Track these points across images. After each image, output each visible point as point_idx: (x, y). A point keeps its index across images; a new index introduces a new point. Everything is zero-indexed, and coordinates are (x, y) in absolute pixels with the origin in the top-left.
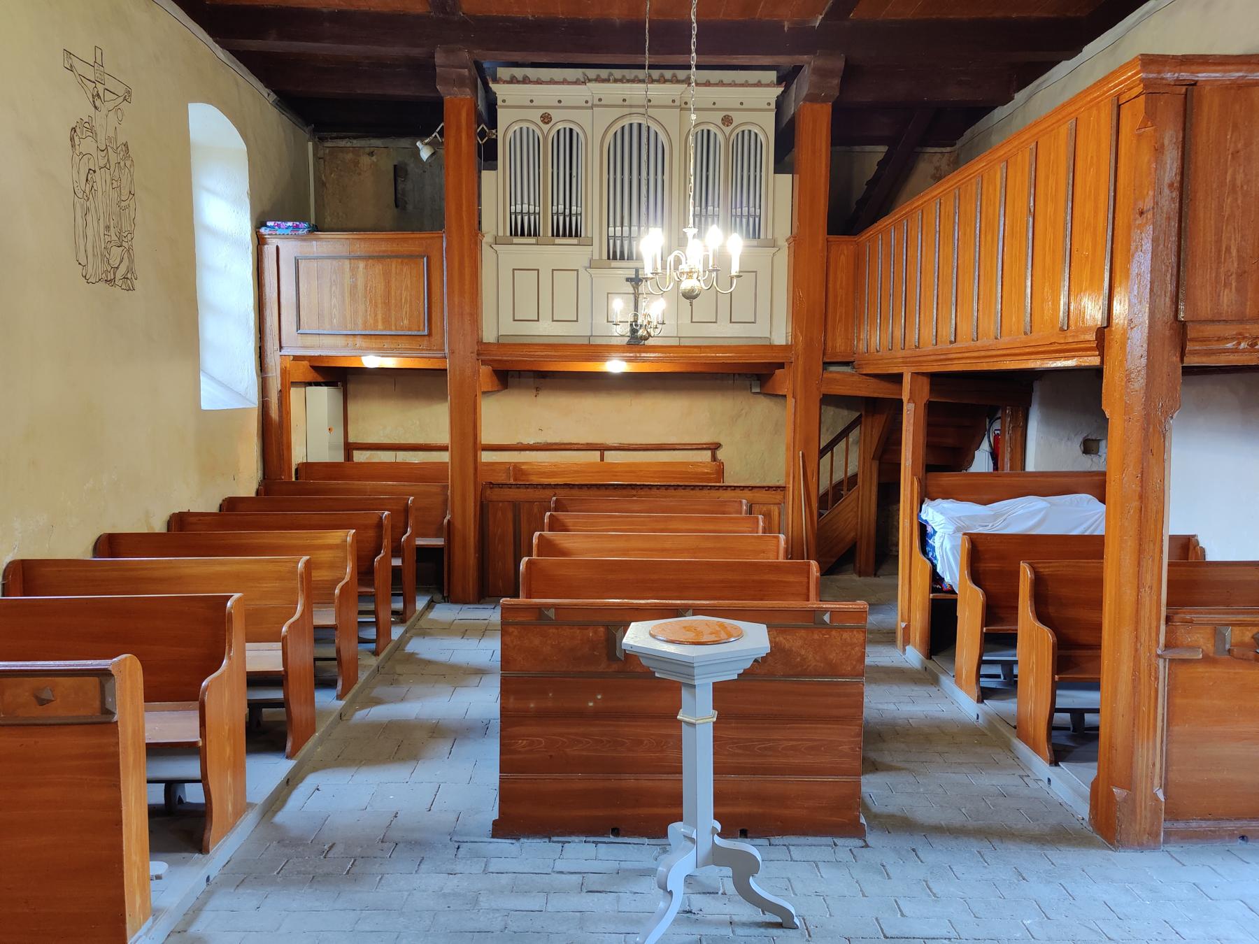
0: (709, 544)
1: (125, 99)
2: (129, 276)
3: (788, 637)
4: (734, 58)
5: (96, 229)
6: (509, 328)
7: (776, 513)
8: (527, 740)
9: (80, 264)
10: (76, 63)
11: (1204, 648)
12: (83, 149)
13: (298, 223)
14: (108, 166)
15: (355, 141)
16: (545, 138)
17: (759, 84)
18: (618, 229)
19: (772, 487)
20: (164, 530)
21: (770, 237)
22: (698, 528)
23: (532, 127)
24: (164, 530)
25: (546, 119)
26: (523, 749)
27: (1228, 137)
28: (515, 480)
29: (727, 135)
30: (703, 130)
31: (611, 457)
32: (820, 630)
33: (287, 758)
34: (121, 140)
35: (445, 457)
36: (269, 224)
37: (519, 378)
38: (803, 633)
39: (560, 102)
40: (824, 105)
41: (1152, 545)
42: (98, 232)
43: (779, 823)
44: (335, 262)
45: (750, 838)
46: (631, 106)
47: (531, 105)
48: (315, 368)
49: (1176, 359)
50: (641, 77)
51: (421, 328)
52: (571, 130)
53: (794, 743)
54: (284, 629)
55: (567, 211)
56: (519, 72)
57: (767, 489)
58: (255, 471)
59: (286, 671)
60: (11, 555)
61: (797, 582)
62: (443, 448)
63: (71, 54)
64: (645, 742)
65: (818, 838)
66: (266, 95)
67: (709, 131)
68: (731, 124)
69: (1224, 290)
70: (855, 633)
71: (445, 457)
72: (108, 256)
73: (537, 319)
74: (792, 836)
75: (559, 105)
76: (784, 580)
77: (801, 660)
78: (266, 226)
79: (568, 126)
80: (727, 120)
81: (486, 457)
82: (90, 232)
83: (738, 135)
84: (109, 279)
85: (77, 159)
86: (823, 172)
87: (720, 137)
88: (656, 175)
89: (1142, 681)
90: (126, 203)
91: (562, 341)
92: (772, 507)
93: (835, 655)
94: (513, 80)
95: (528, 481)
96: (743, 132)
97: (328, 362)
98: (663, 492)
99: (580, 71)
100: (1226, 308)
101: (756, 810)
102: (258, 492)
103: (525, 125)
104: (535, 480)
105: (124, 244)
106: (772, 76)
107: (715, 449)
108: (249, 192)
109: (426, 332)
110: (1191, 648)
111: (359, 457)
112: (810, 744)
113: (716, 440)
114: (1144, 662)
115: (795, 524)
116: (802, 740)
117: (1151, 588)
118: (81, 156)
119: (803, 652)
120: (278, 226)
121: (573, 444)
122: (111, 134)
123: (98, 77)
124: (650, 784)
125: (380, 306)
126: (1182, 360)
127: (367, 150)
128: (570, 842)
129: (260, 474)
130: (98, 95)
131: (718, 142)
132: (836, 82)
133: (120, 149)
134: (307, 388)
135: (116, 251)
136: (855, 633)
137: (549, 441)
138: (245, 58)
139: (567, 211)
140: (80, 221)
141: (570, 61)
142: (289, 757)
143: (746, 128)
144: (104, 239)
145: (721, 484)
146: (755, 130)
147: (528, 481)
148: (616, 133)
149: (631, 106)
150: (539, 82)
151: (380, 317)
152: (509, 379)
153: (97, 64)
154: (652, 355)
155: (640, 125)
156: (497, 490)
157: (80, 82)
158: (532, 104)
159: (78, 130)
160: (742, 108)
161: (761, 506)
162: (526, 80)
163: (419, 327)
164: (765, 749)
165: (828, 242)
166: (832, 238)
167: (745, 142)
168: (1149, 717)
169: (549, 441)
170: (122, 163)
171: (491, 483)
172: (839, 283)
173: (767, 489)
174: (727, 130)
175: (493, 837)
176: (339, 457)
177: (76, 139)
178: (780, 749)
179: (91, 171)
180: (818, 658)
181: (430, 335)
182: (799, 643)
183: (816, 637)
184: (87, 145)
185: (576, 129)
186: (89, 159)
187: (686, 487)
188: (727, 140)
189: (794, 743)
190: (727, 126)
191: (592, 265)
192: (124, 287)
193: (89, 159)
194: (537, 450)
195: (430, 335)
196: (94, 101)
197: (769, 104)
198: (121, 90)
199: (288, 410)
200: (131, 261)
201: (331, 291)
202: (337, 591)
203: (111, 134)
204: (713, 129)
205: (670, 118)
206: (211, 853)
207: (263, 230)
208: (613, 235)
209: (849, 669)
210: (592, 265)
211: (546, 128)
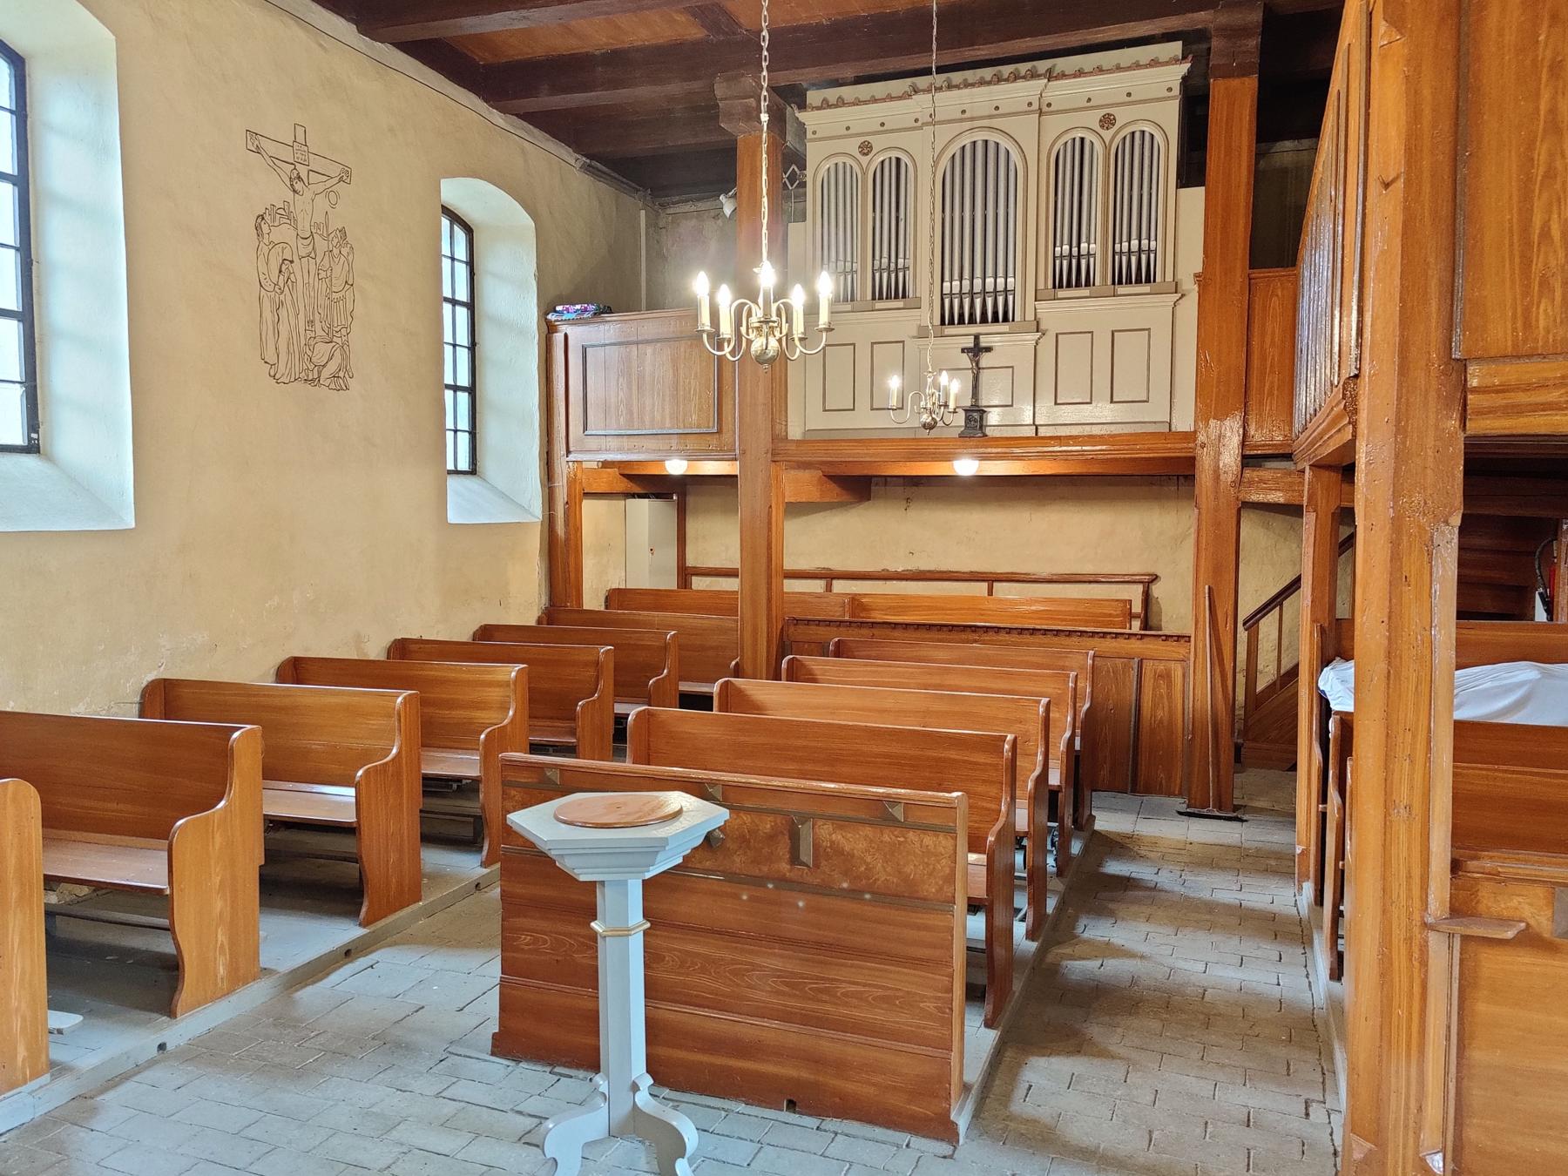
0: (943, 707)
1: (341, 180)
2: (341, 374)
3: (849, 835)
4: (1096, 33)
5: (293, 324)
6: (819, 421)
7: (1179, 673)
8: (531, 936)
9: (266, 362)
10: (265, 144)
11: (1532, 922)
12: (276, 235)
13: (586, 305)
14: (313, 255)
15: (700, 204)
16: (864, 173)
17: (1155, 63)
18: (956, 283)
19: (1172, 636)
20: (383, 657)
21: (1169, 278)
22: (983, 685)
23: (849, 161)
24: (383, 657)
25: (866, 149)
26: (526, 948)
27: (1542, 38)
28: (853, 615)
30: (1074, 139)
31: (839, 586)
32: (893, 829)
33: (360, 925)
34: (335, 224)
35: (731, 584)
36: (559, 308)
37: (886, 485)
38: (868, 831)
40: (1246, 79)
41: (1409, 736)
42: (297, 326)
43: (837, 1100)
44: (622, 349)
45: (798, 1113)
46: (972, 119)
47: (848, 132)
48: (630, 478)
49: (1453, 423)
50: (988, 78)
51: (711, 425)
52: (898, 160)
53: (861, 989)
54: (360, 773)
55: (893, 266)
56: (832, 94)
57: (1164, 638)
58: (537, 595)
59: (358, 822)
60: (155, 673)
61: (990, 765)
62: (731, 573)
63: (257, 134)
64: (667, 959)
65: (890, 1132)
66: (573, 162)
67: (1082, 140)
69: (1540, 297)
70: (941, 838)
71: (731, 584)
72: (310, 354)
73: (852, 407)
74: (855, 1122)
75: (882, 129)
76: (972, 759)
77: (866, 869)
78: (556, 311)
79: (894, 154)
80: (1108, 121)
81: (792, 586)
82: (283, 328)
83: (1125, 138)
84: (310, 378)
85: (266, 250)
86: (1244, 180)
87: (1098, 147)
89: (1396, 964)
90: (340, 294)
91: (875, 435)
92: (1172, 665)
93: (912, 867)
94: (825, 105)
95: (869, 618)
96: (1133, 134)
97: (638, 469)
98: (1014, 638)
99: (909, 81)
100: (1542, 332)
101: (805, 1075)
102: (539, 621)
103: (840, 160)
104: (879, 617)
105: (335, 339)
106: (1176, 48)
107: (1149, 583)
108: (537, 274)
109: (715, 430)
110: (1504, 921)
111: (698, 583)
112: (880, 992)
113: (1151, 571)
114: (1398, 934)
115: (1198, 692)
116: (870, 985)
117: (1409, 807)
118: (270, 247)
119: (869, 859)
120: (567, 310)
121: (953, 572)
122: (319, 218)
123: (298, 158)
124: (672, 1016)
125: (667, 399)
126: (1464, 428)
127: (713, 213)
128: (571, 1077)
129: (544, 600)
130: (299, 178)
131: (1095, 153)
132: (1253, 43)
133: (332, 235)
134: (627, 501)
135: (322, 351)
136: (941, 838)
137: (944, 568)
138: (535, 119)
139: (893, 266)
140: (267, 314)
141: (879, 70)
142: (363, 925)
143: (1137, 128)
144: (305, 335)
145: (1127, 631)
146: (1148, 128)
147: (869, 618)
148: (953, 156)
149: (972, 119)
150: (857, 102)
151: (667, 411)
152: (873, 488)
153: (300, 143)
154: (994, 450)
155: (844, 163)
156: (801, 628)
157: (272, 164)
159: (267, 217)
160: (1130, 99)
161: (1156, 663)
162: (841, 103)
163: (708, 424)
164: (820, 991)
165: (1250, 279)
166: (1256, 273)
167: (1136, 146)
168: (1409, 1028)
169: (922, 568)
170: (336, 251)
171: (794, 619)
172: (1268, 340)
173: (1164, 638)
174: (1107, 135)
175: (493, 1054)
176: (670, 582)
177: (265, 228)
178: (839, 994)
179: (286, 262)
180: (889, 869)
181: (720, 432)
182: (862, 845)
183: (886, 838)
184: (283, 233)
185: (905, 159)
186: (283, 249)
187: (1046, 631)
188: (1107, 148)
189: (861, 989)
190: (1107, 129)
191: (922, 334)
192: (332, 386)
193: (283, 249)
194: (907, 580)
195: (720, 432)
196: (292, 185)
197: (1170, 89)
198: (335, 171)
199: (578, 524)
200: (346, 357)
201: (618, 380)
202: (483, 736)
203: (319, 218)
204: (1089, 137)
205: (1024, 129)
206: (178, 1019)
207: (552, 317)
208: (949, 292)
209: (933, 890)
210: (922, 334)
211: (864, 160)
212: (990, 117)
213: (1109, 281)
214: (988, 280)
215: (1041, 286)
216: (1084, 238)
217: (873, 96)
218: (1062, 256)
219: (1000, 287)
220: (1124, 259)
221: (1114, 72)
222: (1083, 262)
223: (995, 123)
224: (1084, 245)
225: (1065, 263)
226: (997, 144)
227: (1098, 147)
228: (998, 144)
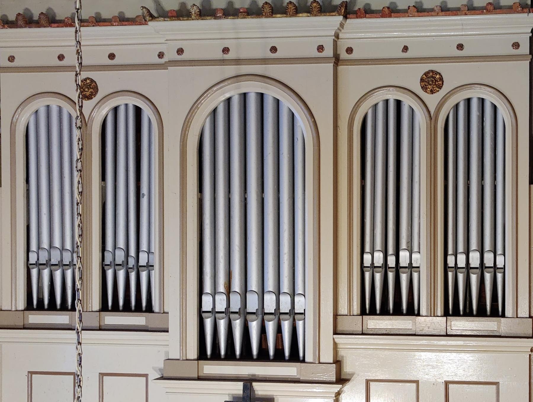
29: (432, 111)
39: (274, 49)
46: (238, 62)
68: (440, 87)
79: (392, 96)
83: (457, 106)
87: (421, 118)
88: (229, 192)
96: (468, 101)
143: (475, 94)
146: (490, 98)
149: (238, 62)
155: (126, 105)
158: (61, 63)
185: (147, 112)
188: (432, 118)
190: (432, 92)
197: (516, 45)
212: (264, 61)
213: (440, 310)
214: (267, 297)
215: (343, 309)
216: (403, 244)
217: (98, 14)
218: (373, 266)
219: (285, 307)
220: (461, 277)
221: (437, 15)
222: (404, 278)
223: (273, 70)
224: (404, 255)
225: (378, 277)
226: (277, 102)
227: (421, 118)
228: (60, 106)
